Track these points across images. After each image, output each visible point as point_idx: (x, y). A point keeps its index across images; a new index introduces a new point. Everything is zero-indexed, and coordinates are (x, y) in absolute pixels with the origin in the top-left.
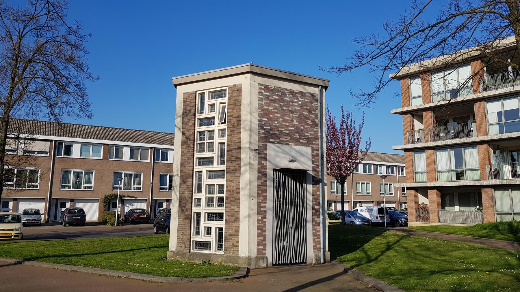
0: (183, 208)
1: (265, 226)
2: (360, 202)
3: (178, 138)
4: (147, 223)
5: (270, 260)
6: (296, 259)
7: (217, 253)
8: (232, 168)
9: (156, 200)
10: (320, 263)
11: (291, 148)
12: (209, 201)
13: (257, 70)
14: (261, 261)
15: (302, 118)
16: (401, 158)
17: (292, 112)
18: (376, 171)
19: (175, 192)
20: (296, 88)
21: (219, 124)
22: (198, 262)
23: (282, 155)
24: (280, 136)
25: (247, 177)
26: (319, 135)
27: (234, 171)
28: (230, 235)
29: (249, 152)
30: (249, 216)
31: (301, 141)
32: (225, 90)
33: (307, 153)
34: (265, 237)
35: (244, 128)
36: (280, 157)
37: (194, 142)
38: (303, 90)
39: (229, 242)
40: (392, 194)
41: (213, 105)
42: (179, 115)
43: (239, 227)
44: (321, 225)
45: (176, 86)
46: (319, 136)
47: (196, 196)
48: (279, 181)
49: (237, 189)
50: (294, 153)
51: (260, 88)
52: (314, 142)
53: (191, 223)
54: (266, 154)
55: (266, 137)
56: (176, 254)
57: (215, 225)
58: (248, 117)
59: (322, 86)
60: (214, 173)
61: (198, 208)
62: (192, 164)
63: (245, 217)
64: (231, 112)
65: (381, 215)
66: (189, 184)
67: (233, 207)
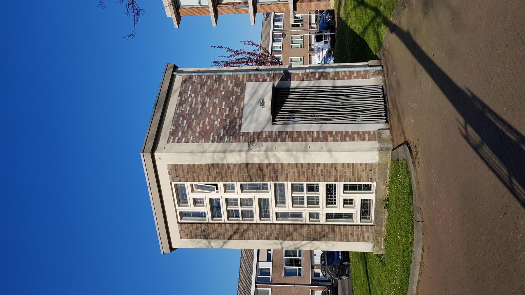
0: (322, 235)
1: (341, 133)
2: (310, 45)
3: (237, 244)
4: (336, 289)
5: (382, 126)
6: (379, 97)
7: (375, 191)
8: (272, 174)
9: (312, 280)
10: (383, 70)
11: (246, 105)
12: (313, 203)
13: (150, 145)
14: (383, 136)
15: (212, 93)
16: (265, 28)
17: (204, 104)
18: (279, 52)
19: (302, 246)
20: (174, 100)
21: (217, 192)
22: (386, 215)
23: (255, 116)
24: (232, 118)
25: (282, 154)
26: (232, 73)
27: (275, 171)
29: (251, 153)
30: (329, 151)
31: (239, 94)
32: (176, 185)
33: (254, 87)
34: (353, 133)
35: (222, 160)
36: (257, 115)
37: (241, 224)
38: (178, 93)
39: (361, 176)
40: (301, 37)
41: (196, 202)
42: (208, 244)
43: (343, 164)
44: (338, 70)
45: (172, 249)
46: (234, 73)
47: (306, 219)
48: (287, 118)
49: (297, 167)
50: (254, 102)
51: (173, 142)
52: (241, 80)
53: (339, 225)
54: (254, 132)
55: (234, 134)
56: (376, 243)
57: (341, 195)
58: (209, 155)
59: (174, 71)
60: (278, 198)
61: (320, 216)
62: (268, 225)
63: (331, 156)
64: (203, 177)
65: (323, 38)
66: (291, 229)
67: (319, 172)
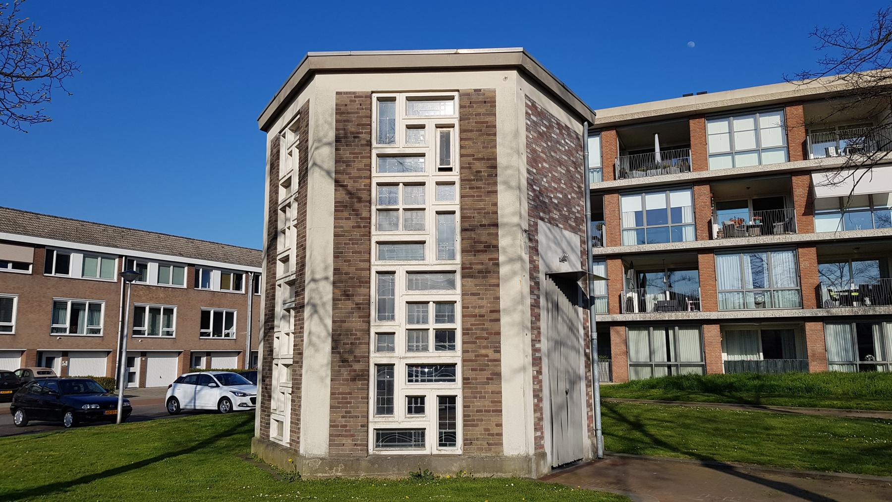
28: (477, 411)
35: (506, 183)
39: (476, 426)
42: (325, 140)
49: (492, 312)
57: (432, 392)
67: (483, 352)
